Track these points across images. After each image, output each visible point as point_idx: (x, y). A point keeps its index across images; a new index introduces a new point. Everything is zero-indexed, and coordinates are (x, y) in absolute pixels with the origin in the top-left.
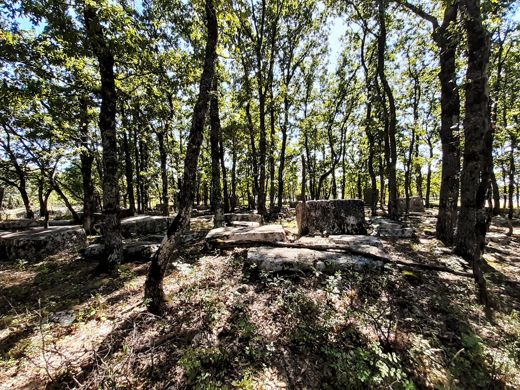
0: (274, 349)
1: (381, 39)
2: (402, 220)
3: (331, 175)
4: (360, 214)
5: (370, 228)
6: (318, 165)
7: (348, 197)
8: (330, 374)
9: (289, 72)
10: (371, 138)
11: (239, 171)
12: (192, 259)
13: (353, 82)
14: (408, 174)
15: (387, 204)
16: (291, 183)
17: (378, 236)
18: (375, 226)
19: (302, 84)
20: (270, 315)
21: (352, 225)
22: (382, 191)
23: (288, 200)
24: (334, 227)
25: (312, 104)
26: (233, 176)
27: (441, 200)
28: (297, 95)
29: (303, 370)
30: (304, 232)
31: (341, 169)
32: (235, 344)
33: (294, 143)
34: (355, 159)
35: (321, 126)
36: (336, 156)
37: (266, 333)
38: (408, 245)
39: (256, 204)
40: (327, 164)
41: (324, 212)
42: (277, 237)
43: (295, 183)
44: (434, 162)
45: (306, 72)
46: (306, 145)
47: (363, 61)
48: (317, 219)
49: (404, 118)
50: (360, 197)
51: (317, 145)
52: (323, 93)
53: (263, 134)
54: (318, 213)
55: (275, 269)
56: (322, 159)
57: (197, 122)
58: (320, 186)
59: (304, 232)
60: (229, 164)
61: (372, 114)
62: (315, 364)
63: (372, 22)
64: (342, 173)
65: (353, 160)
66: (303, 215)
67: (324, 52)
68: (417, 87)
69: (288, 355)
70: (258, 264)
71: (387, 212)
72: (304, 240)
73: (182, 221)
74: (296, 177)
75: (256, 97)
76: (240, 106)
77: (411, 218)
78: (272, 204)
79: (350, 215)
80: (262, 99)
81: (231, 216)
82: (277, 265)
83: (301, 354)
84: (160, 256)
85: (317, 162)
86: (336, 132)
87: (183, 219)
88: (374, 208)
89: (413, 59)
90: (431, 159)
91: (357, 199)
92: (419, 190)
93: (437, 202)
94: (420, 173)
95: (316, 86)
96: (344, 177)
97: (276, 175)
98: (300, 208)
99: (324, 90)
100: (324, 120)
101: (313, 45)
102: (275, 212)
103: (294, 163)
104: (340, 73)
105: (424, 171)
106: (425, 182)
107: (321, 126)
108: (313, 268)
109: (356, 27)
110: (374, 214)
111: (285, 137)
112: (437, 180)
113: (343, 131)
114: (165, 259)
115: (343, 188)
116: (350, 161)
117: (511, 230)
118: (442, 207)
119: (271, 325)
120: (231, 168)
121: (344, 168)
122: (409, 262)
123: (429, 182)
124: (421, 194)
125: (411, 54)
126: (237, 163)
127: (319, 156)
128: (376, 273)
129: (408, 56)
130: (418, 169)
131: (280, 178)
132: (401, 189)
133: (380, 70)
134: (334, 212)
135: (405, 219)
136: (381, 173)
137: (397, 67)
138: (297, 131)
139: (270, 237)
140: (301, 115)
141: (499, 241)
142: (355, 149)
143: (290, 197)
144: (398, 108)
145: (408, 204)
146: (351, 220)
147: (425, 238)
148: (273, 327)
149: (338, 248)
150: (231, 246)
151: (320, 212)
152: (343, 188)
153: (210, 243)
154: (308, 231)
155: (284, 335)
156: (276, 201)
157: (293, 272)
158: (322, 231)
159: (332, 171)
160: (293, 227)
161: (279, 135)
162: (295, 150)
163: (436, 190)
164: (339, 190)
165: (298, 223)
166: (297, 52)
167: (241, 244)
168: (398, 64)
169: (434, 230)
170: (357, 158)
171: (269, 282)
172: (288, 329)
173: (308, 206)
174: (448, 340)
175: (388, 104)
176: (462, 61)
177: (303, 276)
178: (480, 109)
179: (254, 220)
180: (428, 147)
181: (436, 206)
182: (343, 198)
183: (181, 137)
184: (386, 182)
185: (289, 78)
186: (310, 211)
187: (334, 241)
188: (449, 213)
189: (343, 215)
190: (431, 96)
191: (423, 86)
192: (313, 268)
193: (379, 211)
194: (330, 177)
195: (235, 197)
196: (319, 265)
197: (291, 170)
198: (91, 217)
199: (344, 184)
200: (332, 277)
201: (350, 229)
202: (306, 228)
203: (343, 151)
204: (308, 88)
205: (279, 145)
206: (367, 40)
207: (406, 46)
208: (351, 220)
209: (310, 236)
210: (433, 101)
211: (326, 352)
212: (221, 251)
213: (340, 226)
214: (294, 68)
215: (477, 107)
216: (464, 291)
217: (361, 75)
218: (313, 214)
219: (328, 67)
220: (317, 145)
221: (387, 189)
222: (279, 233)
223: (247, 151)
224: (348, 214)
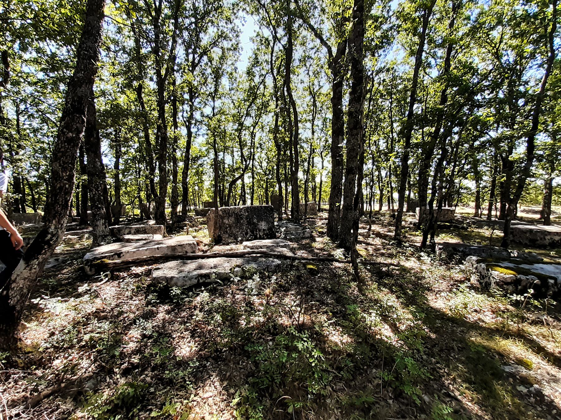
0: (197, 364)
1: (288, 50)
3: (240, 181)
4: (271, 219)
5: (278, 232)
6: (228, 170)
7: (256, 203)
8: (254, 368)
9: (194, 59)
10: (278, 146)
11: (124, 171)
12: (66, 290)
13: (262, 87)
14: (307, 181)
15: (290, 209)
16: (196, 188)
17: (285, 238)
18: (283, 230)
19: (210, 76)
20: (187, 333)
21: (264, 230)
22: (286, 197)
23: (192, 208)
24: (247, 234)
25: (220, 101)
26: (116, 177)
27: (331, 205)
28: (204, 87)
29: (228, 374)
30: (217, 241)
31: (250, 174)
32: (147, 375)
33: (200, 143)
34: (263, 165)
35: (230, 127)
36: (246, 161)
37: (184, 352)
38: (308, 244)
39: (151, 213)
40: (237, 169)
41: (238, 219)
42: (188, 249)
43: (201, 189)
44: (325, 173)
45: (214, 63)
46: (214, 147)
47: (272, 69)
48: (230, 226)
49: (304, 133)
50: (267, 203)
51: (226, 148)
52: (233, 92)
53: (162, 129)
54: (232, 220)
55: (189, 284)
56: (231, 163)
57: (74, 101)
58: (230, 191)
59: (217, 241)
60: (108, 160)
61: (279, 123)
62: (239, 364)
63: (281, 32)
64: (251, 179)
65: (261, 167)
66: (216, 223)
67: (235, 49)
68: (314, 105)
69: (212, 365)
70: (167, 281)
72: (218, 249)
73: (51, 239)
74: (202, 182)
75: (151, 79)
76: (129, 86)
78: (174, 212)
79: (262, 221)
80: (161, 82)
81: (119, 230)
82: (191, 279)
83: (224, 360)
84: (11, 293)
85: (226, 166)
86: (246, 136)
87: (53, 235)
88: (280, 214)
89: (313, 77)
90: (323, 169)
91: (264, 205)
92: (314, 197)
93: (327, 207)
94: (315, 182)
95: (225, 81)
96: (253, 183)
97: (180, 177)
98: (212, 216)
99: (232, 89)
100: (234, 122)
101: (222, 36)
102: (179, 222)
103: (201, 165)
104: (250, 73)
105: (318, 180)
106: (318, 190)
107: (230, 127)
108: (231, 275)
109: (267, 33)
110: (280, 219)
111: (189, 134)
112: (327, 189)
113: (253, 135)
114: (22, 296)
115: (253, 193)
116: (258, 167)
117: (370, 227)
118: (331, 211)
119: (189, 342)
121: (253, 174)
122: (310, 257)
123: (320, 188)
124: (315, 200)
125: (311, 74)
126: (121, 161)
127: (228, 160)
128: (286, 271)
129: (308, 74)
130: (314, 177)
131: (185, 183)
132: (301, 195)
133: (287, 81)
134: (247, 219)
135: (305, 222)
136: (286, 180)
138: (204, 129)
139: (180, 250)
140: (208, 111)
142: (263, 155)
143: (195, 205)
144: (300, 121)
145: (306, 209)
146: (263, 225)
147: (319, 236)
148: (192, 344)
149: (253, 253)
150: (126, 266)
151: (233, 219)
152: (253, 193)
153: (91, 266)
154: (221, 240)
155: (205, 348)
156: (179, 208)
157: (210, 284)
158: (236, 238)
159: (241, 177)
160: (204, 235)
161: (183, 131)
162: (200, 150)
163: (326, 197)
164: (248, 196)
165: (210, 232)
166: (205, 39)
167: (141, 262)
168: (300, 80)
169: (325, 230)
170: (264, 164)
171: (183, 299)
172: (209, 341)
173: (221, 213)
174: (337, 313)
175: (293, 117)
176: (346, 90)
177: (220, 285)
178: (357, 134)
179: (155, 231)
180: (320, 159)
181: (325, 210)
182: (252, 204)
183: (18, 113)
184: (290, 188)
185: (194, 65)
186: (223, 218)
187: (248, 247)
188: (335, 215)
189: (255, 221)
190: (324, 115)
191: (319, 105)
192: (231, 275)
193: (284, 216)
194: (239, 182)
195: (120, 205)
196: (237, 272)
197: (197, 173)
199: (253, 190)
200: (250, 281)
201: (261, 234)
202: (219, 236)
203: (252, 157)
204: (216, 81)
205: (182, 142)
206: (276, 49)
207: (308, 65)
208: (263, 225)
209: (224, 244)
210: (325, 120)
211: (250, 350)
212: (112, 272)
213: (252, 232)
214: (201, 56)
215: (355, 132)
217: (269, 81)
218: (226, 221)
219: (238, 65)
220: (226, 148)
221: (290, 195)
222: (190, 244)
223: (137, 145)
224: (260, 219)
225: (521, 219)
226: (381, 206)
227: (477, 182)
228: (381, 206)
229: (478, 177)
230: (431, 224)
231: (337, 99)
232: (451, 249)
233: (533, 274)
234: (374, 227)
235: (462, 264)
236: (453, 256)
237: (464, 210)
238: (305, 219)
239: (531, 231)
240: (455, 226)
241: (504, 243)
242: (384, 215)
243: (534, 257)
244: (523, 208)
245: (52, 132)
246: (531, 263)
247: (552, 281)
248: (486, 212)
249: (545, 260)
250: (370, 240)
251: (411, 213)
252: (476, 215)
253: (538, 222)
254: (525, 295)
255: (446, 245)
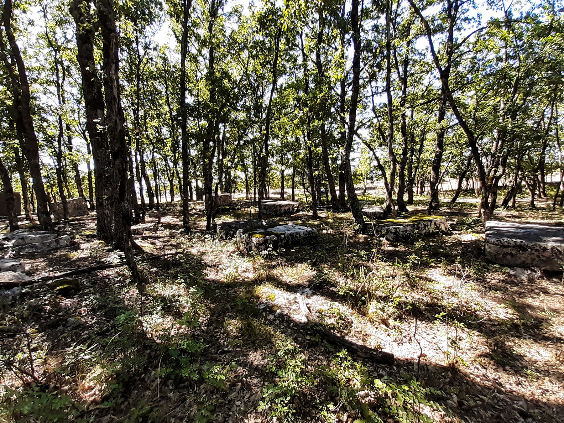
2: (60, 228)
49: (45, 98)
71: (38, 223)
77: (72, 225)
120: (166, 253)
129: (45, 16)
137: (31, 23)
141: (151, 229)
145: (65, 209)
198: (61, 387)
216: (120, 280)
225: (272, 199)
226: (172, 196)
227: (245, 173)
228: (172, 196)
229: (245, 170)
230: (214, 208)
231: (84, 57)
232: (227, 227)
233: (274, 234)
234: (164, 220)
235: (235, 237)
236: (229, 231)
237: (239, 195)
238: (65, 223)
239: (274, 205)
240: (231, 208)
241: (259, 216)
242: (176, 205)
243: (275, 222)
244: (273, 191)
245: (199, 347)
246: (273, 227)
247: (283, 236)
248: (253, 196)
249: (281, 223)
250: (159, 234)
251: (200, 201)
252: (247, 198)
253: (280, 199)
254: (268, 249)
255: (224, 224)
